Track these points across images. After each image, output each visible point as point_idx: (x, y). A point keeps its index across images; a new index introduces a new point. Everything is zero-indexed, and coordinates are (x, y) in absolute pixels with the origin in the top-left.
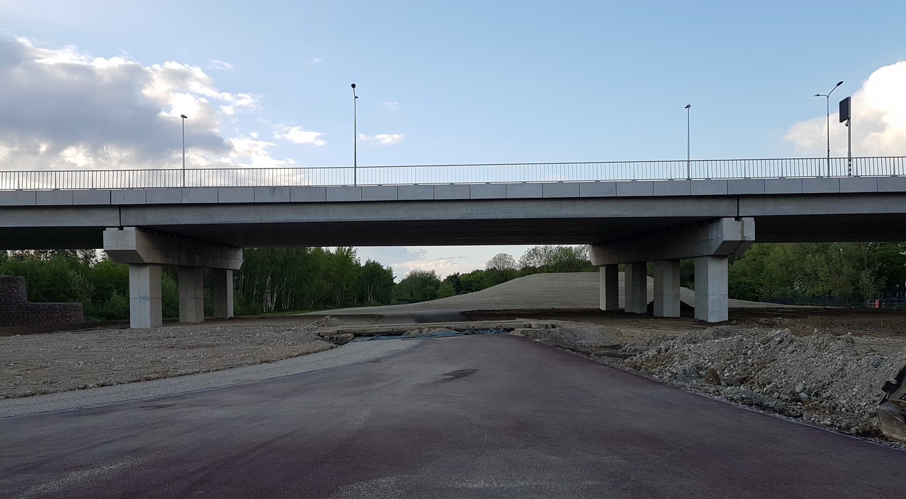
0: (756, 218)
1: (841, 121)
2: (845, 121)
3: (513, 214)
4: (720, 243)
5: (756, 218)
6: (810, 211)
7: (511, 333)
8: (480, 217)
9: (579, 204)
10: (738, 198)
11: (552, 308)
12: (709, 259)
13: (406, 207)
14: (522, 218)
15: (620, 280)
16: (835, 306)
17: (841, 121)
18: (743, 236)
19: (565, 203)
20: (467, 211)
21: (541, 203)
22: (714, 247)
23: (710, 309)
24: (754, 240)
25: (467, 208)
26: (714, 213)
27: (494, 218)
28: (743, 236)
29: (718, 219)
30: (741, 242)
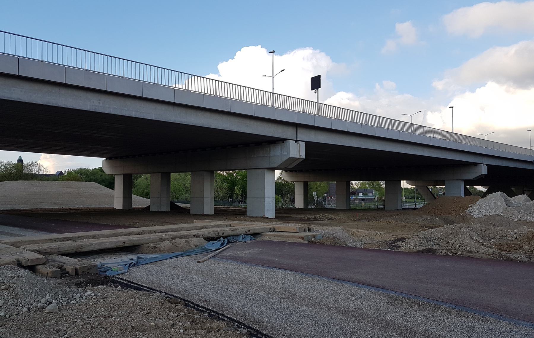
0: (307, 143)
1: (312, 90)
2: (315, 90)
3: (145, 114)
4: (285, 159)
5: (307, 143)
6: (330, 141)
7: (259, 239)
8: (112, 112)
9: (200, 113)
10: (296, 126)
11: (21, 209)
12: (266, 170)
13: (27, 86)
14: (153, 119)
15: (502, 165)
16: (221, 206)
17: (312, 90)
18: (300, 155)
19: (189, 111)
20: (99, 103)
21: (170, 108)
22: (279, 161)
23: (266, 208)
24: (171, 174)
25: (100, 100)
26: (284, 136)
27: (127, 115)
28: (300, 155)
29: (283, 140)
30: (298, 158)
